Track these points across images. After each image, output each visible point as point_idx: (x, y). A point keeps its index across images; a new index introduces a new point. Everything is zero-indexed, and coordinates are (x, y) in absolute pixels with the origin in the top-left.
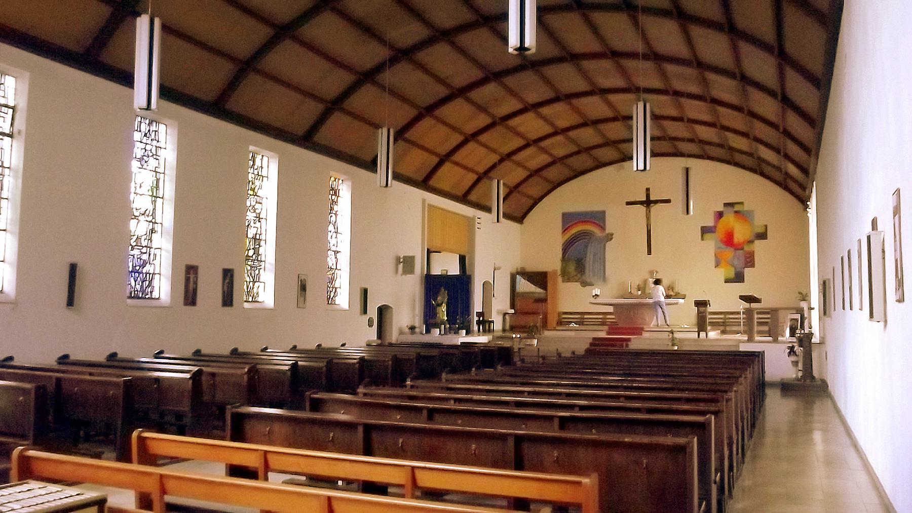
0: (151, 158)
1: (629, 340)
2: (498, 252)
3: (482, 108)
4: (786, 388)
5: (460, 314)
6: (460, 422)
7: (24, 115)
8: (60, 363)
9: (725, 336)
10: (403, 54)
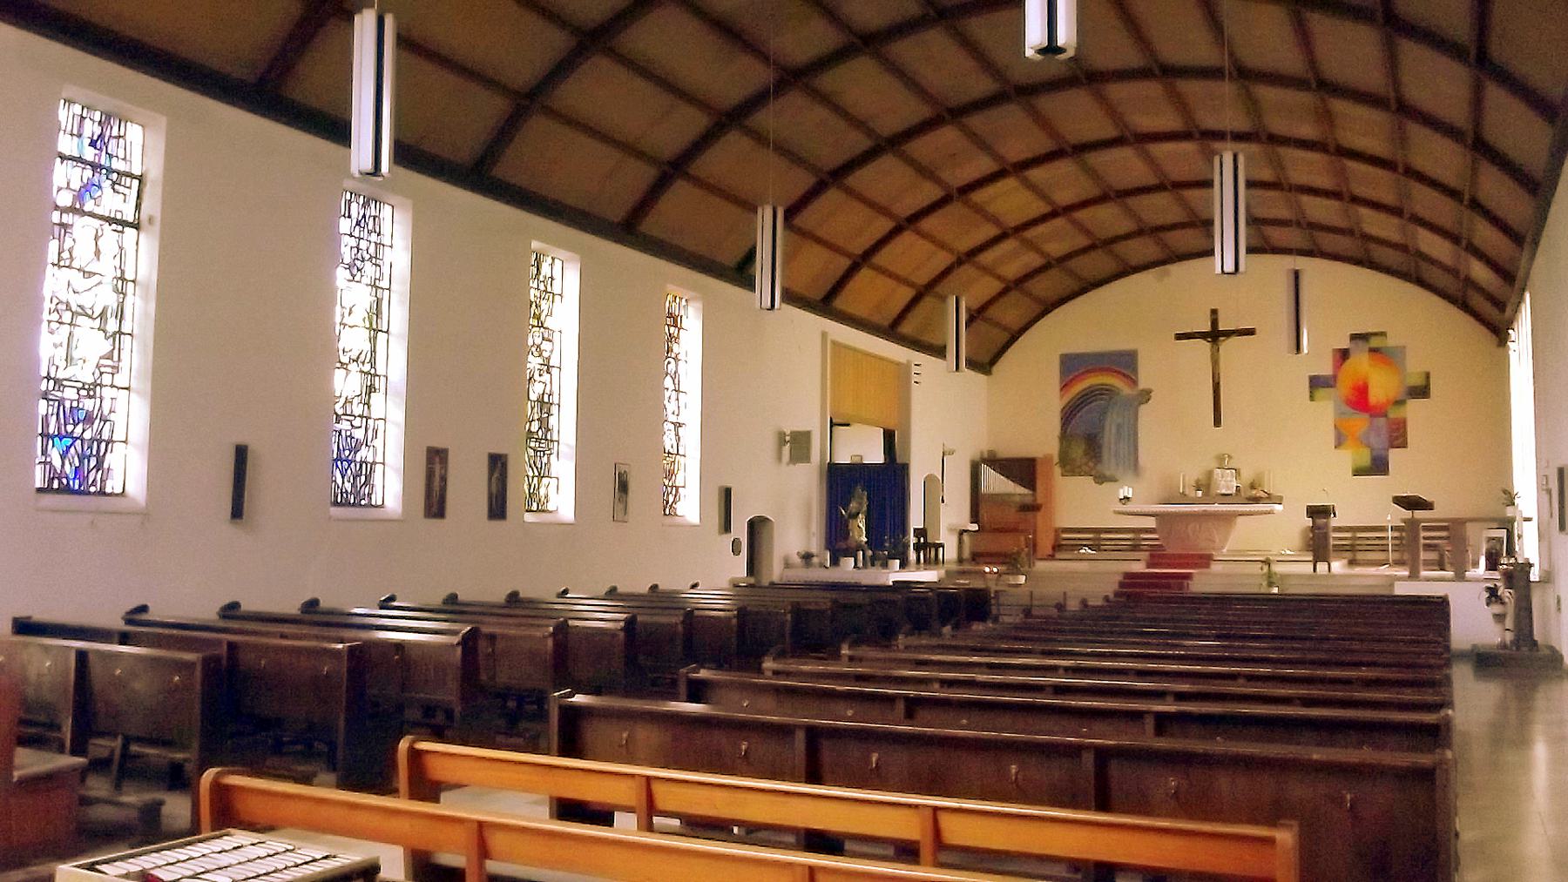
0: (368, 264)
1: (1188, 577)
2: (951, 423)
3: (926, 172)
4: (1485, 661)
5: (889, 531)
6: (850, 713)
7: (159, 190)
8: (129, 622)
9: (1358, 570)
10: (795, 78)
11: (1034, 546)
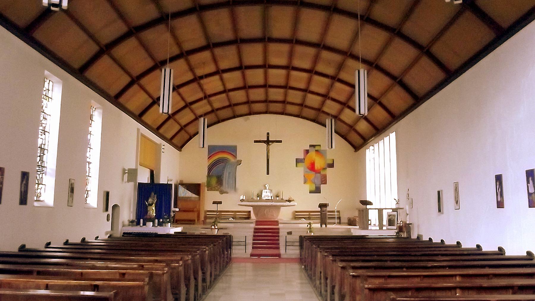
11: (198, 219)
